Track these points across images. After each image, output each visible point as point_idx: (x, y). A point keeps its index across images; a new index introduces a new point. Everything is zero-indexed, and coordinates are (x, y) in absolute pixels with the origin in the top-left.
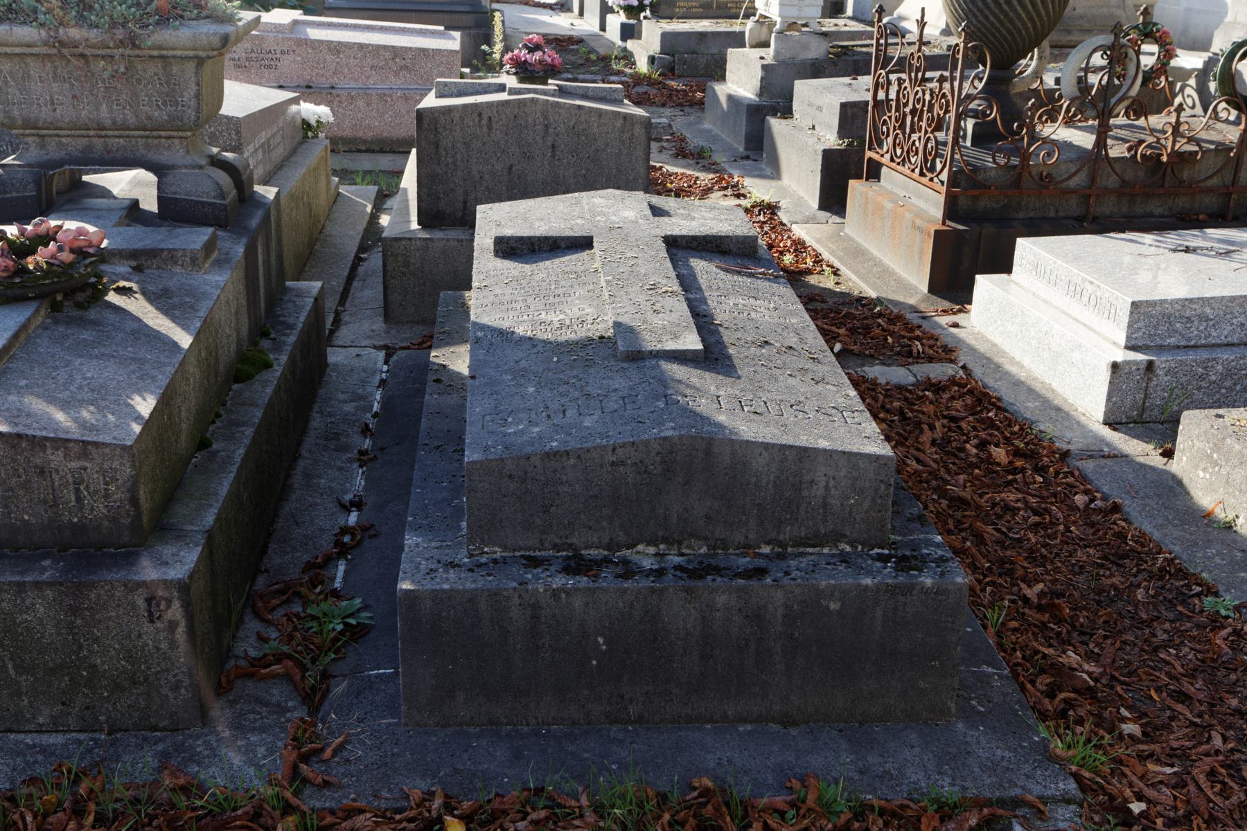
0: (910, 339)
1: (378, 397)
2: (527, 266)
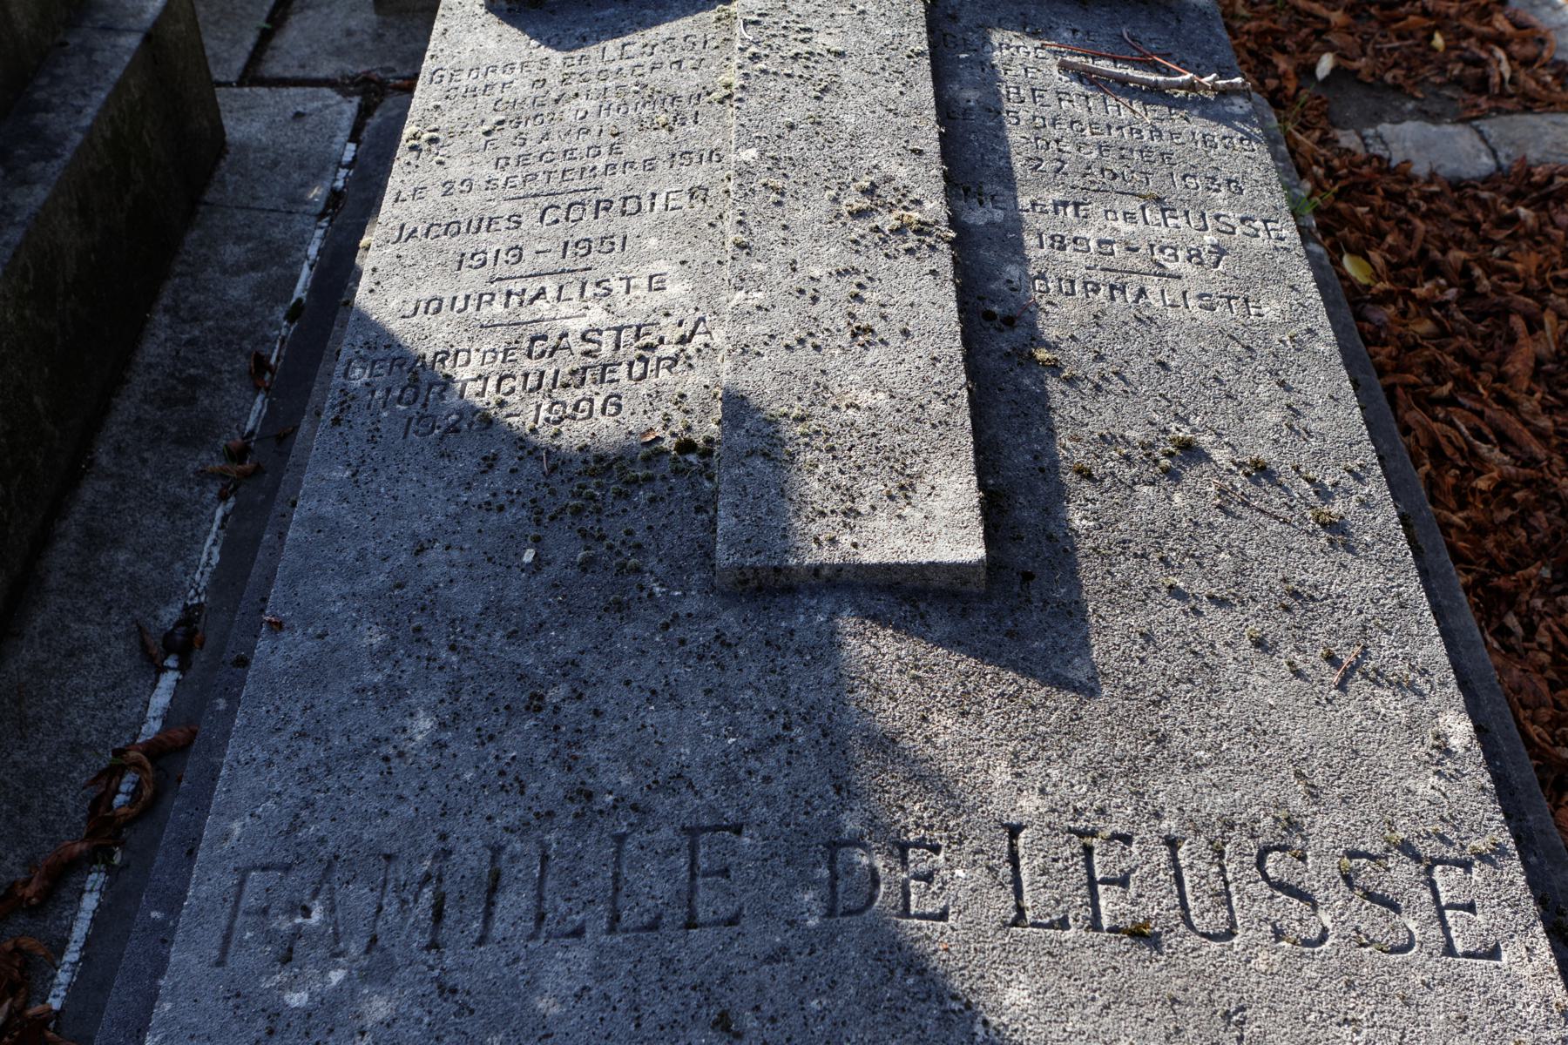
0: (1484, 41)
1: (313, 251)
2: (557, 57)
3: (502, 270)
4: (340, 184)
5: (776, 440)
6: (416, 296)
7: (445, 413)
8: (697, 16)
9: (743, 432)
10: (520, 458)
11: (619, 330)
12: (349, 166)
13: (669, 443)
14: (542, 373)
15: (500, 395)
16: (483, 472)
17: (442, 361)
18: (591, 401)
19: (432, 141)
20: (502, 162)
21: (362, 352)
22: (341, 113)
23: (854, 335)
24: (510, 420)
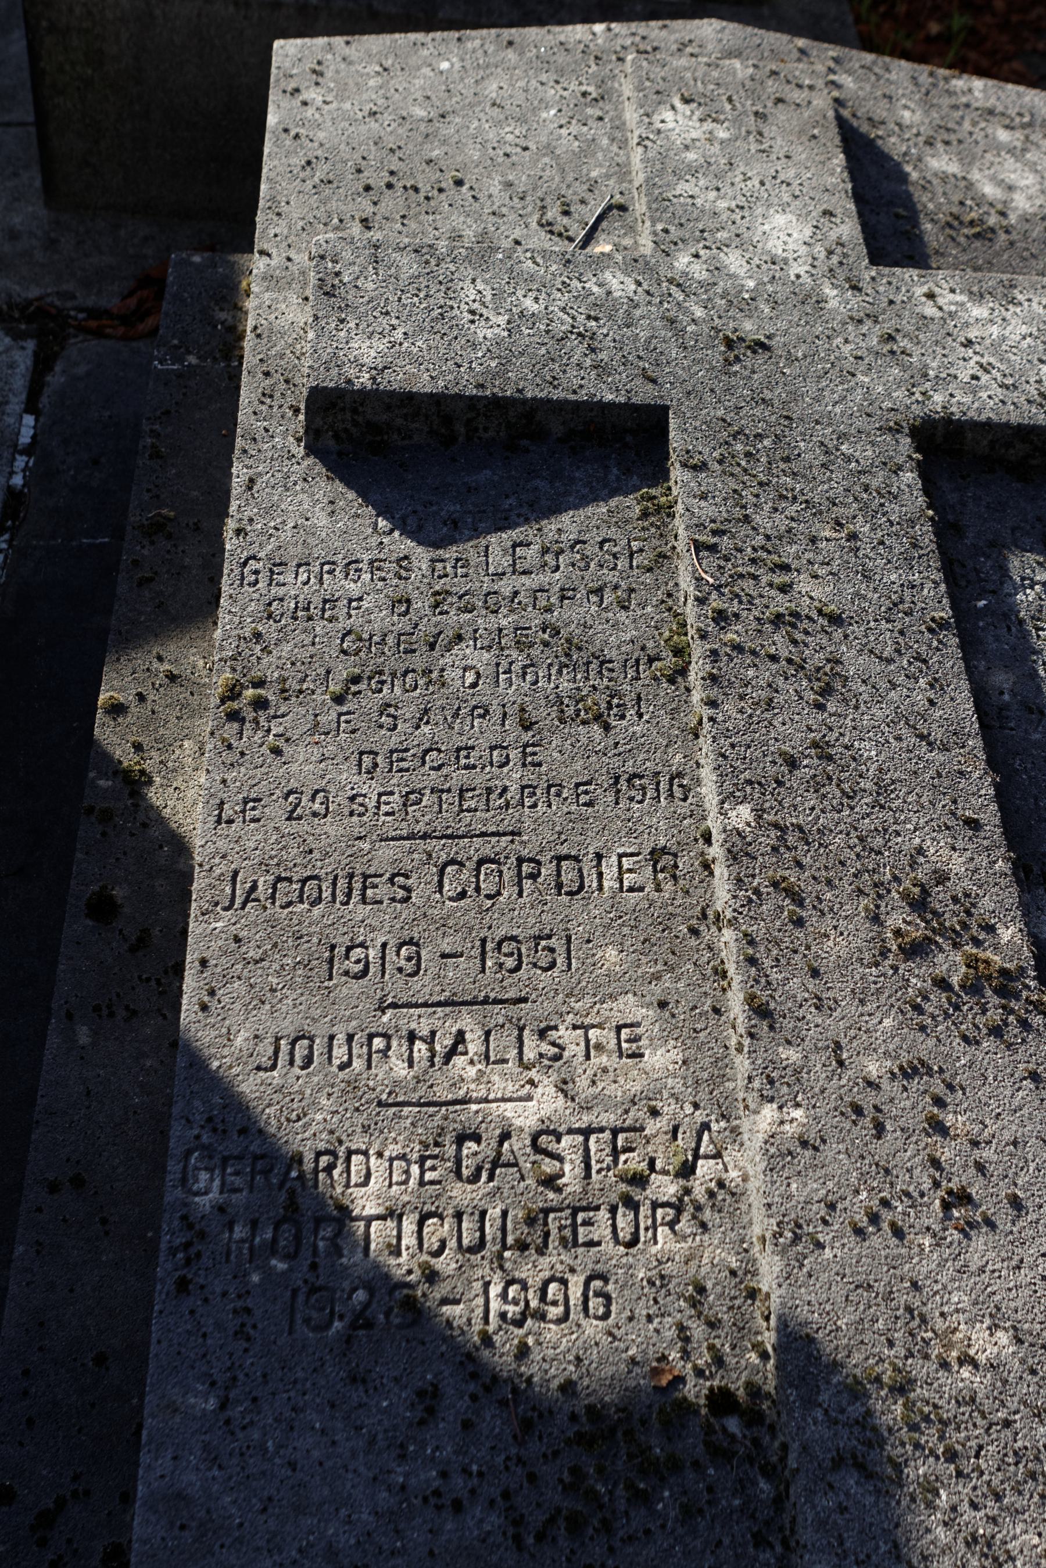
2: (421, 556)
3: (396, 987)
4: (18, 480)
5: (872, 1436)
6: (274, 1029)
7: (346, 1285)
8: (613, 502)
9: (819, 1414)
10: (474, 1398)
11: (587, 1132)
12: (28, 451)
13: (694, 1390)
14: (483, 1214)
15: (425, 1257)
16: (422, 1422)
17: (329, 1169)
18: (564, 1282)
19: (260, 704)
20: (367, 760)
21: (205, 1139)
22: (12, 366)
23: (946, 1206)
24: (447, 1309)
